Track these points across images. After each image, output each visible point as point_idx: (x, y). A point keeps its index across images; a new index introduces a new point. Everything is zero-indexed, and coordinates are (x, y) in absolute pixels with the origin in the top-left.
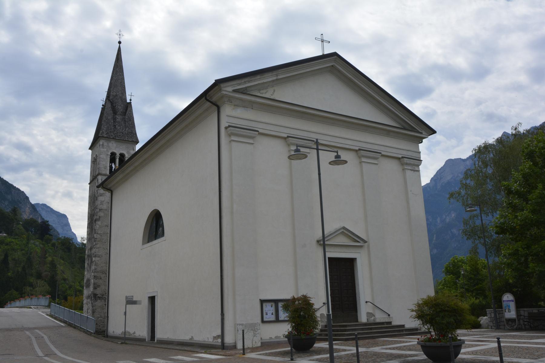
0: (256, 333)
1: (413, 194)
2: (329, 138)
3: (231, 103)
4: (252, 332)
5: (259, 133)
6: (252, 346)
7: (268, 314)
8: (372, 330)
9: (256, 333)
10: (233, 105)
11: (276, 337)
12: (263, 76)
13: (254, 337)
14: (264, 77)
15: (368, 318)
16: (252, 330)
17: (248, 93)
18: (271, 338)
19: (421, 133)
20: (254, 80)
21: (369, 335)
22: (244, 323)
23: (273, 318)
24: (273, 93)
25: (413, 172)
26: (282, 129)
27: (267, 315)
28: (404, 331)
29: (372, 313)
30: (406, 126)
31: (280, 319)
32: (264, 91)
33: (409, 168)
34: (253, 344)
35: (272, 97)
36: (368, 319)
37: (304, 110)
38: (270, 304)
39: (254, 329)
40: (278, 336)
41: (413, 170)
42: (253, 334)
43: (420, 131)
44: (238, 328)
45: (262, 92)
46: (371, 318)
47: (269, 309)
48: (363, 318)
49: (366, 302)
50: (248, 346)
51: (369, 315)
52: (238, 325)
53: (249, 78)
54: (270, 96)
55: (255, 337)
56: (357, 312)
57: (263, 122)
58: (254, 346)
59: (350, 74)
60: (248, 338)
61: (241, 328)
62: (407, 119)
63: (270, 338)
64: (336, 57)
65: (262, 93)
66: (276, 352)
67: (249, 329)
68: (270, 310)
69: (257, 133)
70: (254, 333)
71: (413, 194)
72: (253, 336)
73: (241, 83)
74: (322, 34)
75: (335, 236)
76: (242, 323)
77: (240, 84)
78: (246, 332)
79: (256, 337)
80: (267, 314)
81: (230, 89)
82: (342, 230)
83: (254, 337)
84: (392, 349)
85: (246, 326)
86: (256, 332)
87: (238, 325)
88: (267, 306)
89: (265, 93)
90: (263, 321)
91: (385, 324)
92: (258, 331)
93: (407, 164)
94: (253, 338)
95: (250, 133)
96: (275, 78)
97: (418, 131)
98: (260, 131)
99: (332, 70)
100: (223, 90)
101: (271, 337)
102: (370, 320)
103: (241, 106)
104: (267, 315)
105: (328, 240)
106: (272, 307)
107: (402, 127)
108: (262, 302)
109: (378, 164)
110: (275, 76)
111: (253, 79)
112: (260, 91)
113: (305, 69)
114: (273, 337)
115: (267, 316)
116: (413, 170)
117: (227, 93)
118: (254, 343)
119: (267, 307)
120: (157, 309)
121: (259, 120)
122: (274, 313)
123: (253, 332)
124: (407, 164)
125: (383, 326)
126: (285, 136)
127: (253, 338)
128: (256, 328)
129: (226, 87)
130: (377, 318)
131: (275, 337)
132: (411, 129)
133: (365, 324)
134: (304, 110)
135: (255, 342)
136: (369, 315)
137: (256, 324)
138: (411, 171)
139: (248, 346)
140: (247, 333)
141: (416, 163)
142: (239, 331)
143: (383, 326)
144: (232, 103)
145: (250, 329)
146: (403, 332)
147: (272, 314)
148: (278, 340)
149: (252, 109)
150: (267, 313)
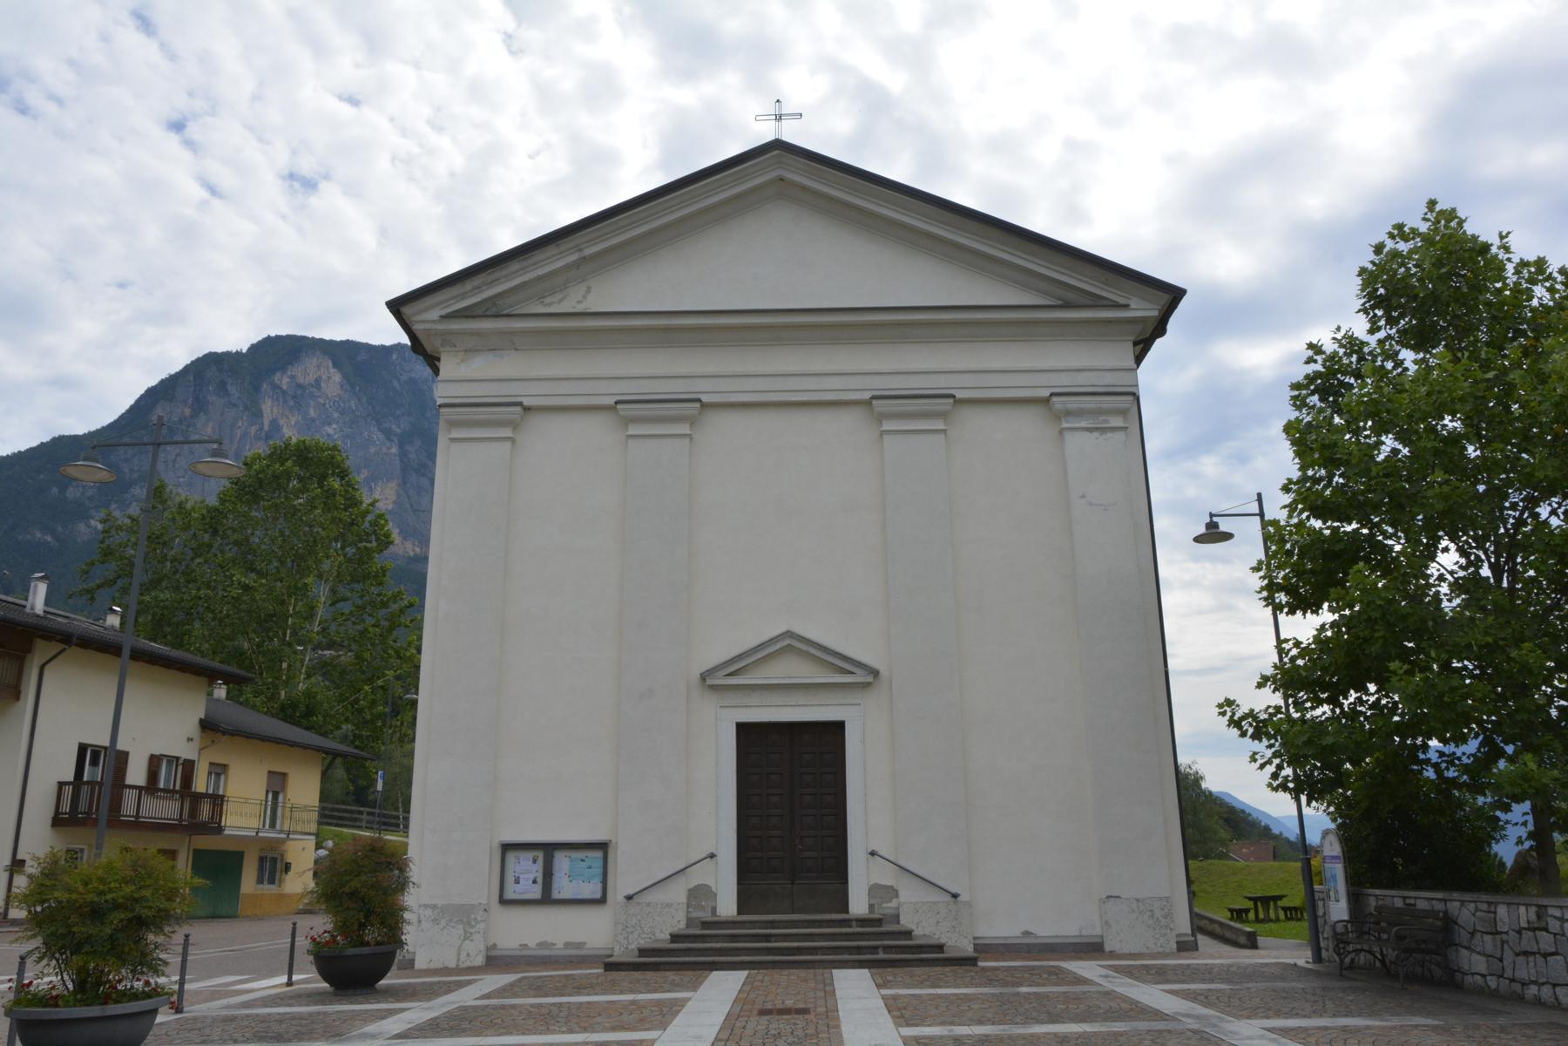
0: (472, 931)
1: (1091, 504)
2: (761, 384)
3: (454, 349)
4: (461, 926)
5: (702, 406)
6: (457, 965)
7: (521, 881)
8: (770, 942)
9: (472, 931)
10: (461, 351)
11: (541, 945)
12: (531, 261)
13: (464, 939)
14: (534, 264)
15: (872, 902)
16: (460, 921)
17: (505, 312)
18: (524, 946)
19: (1126, 306)
20: (506, 276)
21: (677, 957)
22: (440, 903)
23: (536, 892)
24: (584, 297)
25: (1096, 434)
26: (601, 387)
27: (518, 883)
28: (880, 950)
29: (892, 887)
30: (1071, 296)
31: (556, 895)
32: (558, 296)
33: (1083, 424)
34: (458, 960)
35: (580, 308)
36: (871, 907)
37: (664, 322)
38: (530, 855)
39: (465, 920)
40: (546, 942)
41: (1097, 429)
42: (461, 932)
43: (1122, 301)
44: (422, 916)
45: (548, 300)
46: (887, 902)
47: (526, 870)
48: (858, 904)
49: (873, 854)
50: (443, 964)
51: (876, 891)
52: (422, 908)
53: (484, 275)
54: (574, 307)
55: (467, 941)
56: (847, 882)
57: (572, 377)
58: (462, 966)
59: (833, 187)
60: (447, 941)
61: (430, 917)
62: (1062, 273)
63: (521, 945)
64: (776, 152)
65: (551, 304)
66: (424, 982)
67: (451, 920)
68: (527, 872)
69: (951, 400)
70: (465, 931)
71: (1091, 504)
72: (462, 938)
73: (466, 293)
74: (778, 101)
75: (757, 661)
76: (434, 903)
77: (463, 296)
78: (444, 928)
79: (472, 940)
80: (517, 881)
81: (434, 314)
82: (788, 641)
83: (464, 939)
84: (400, 1009)
85: (442, 911)
86: (473, 927)
87: (422, 908)
88: (521, 859)
89: (561, 300)
90: (504, 902)
91: (854, 923)
92: (478, 926)
93: (1068, 413)
94: (461, 945)
95: (668, 409)
96: (574, 257)
97: (1111, 300)
98: (959, 395)
99: (782, 191)
100: (416, 322)
101: (526, 945)
102: (883, 908)
103: (482, 351)
104: (518, 883)
105: (736, 671)
106: (535, 861)
107: (1060, 303)
108: (507, 848)
109: (1127, 428)
110: (575, 252)
111: (497, 275)
112: (544, 300)
113: (677, 210)
114: (532, 944)
115: (519, 888)
116: (1097, 429)
117: (427, 326)
118: (463, 957)
119: (519, 863)
120: (187, 867)
121: (534, 374)
122: (540, 880)
123: (464, 928)
124: (1068, 413)
125: (844, 930)
126: (611, 401)
127: (461, 945)
128: (473, 916)
129: (420, 312)
130: (904, 903)
131: (538, 945)
132: (1090, 303)
133: (862, 921)
134: (664, 322)
135: (466, 954)
136: (876, 891)
137: (473, 906)
138: (1088, 433)
139: (443, 964)
140: (445, 930)
141: (1104, 406)
142: (423, 922)
143: (844, 930)
144: (455, 346)
145: (455, 920)
146: (877, 953)
147: (535, 882)
148: (546, 952)
149: (516, 349)
150: (519, 878)
